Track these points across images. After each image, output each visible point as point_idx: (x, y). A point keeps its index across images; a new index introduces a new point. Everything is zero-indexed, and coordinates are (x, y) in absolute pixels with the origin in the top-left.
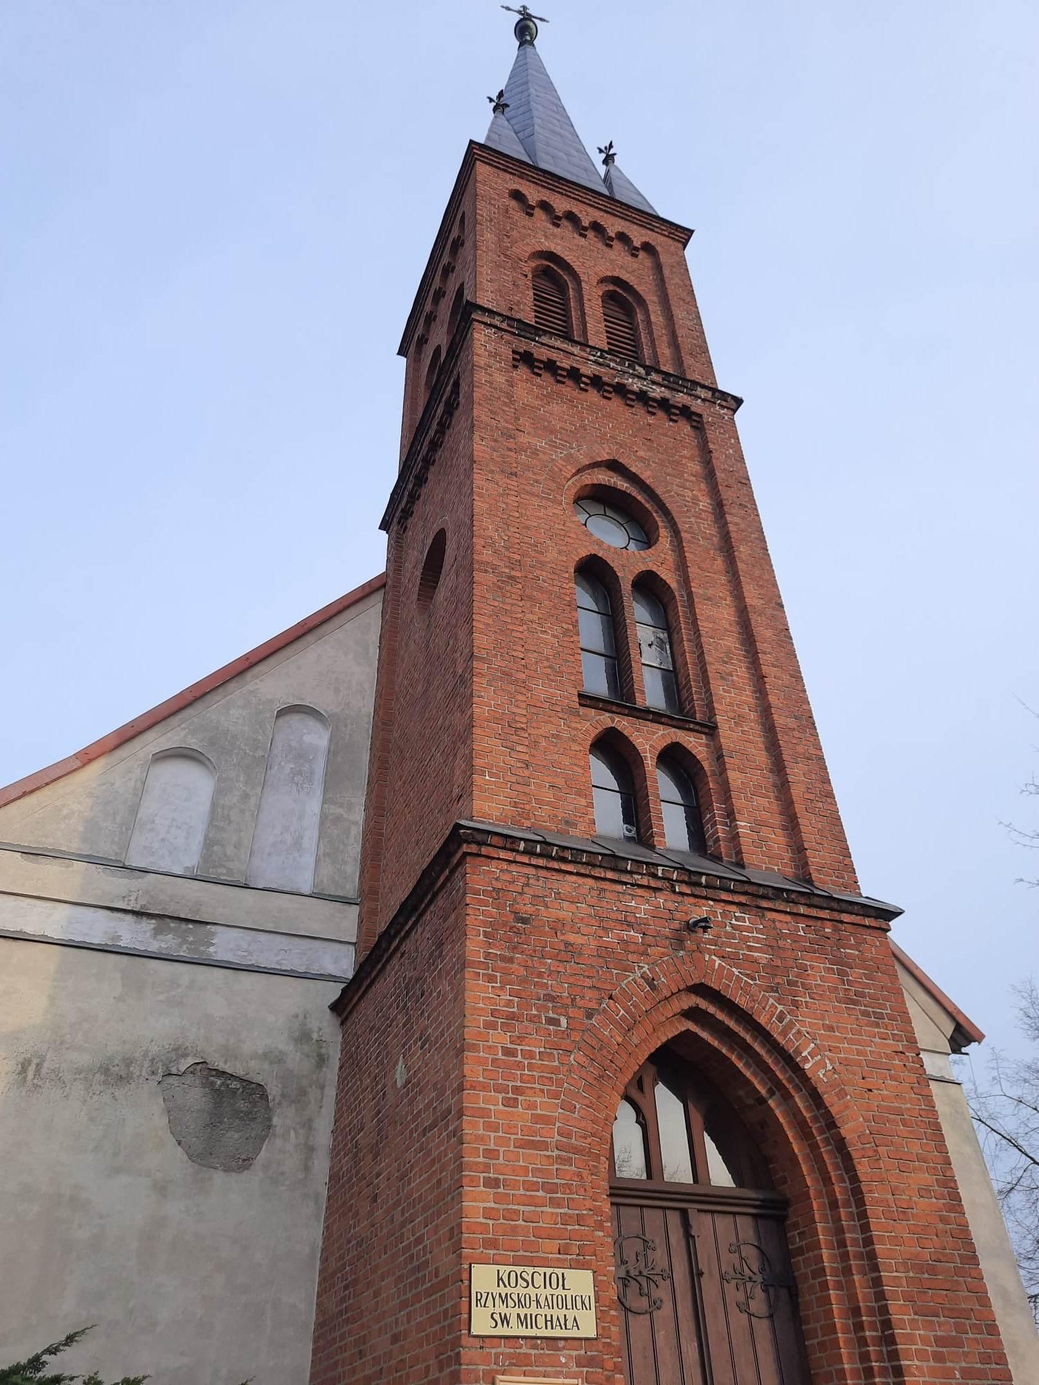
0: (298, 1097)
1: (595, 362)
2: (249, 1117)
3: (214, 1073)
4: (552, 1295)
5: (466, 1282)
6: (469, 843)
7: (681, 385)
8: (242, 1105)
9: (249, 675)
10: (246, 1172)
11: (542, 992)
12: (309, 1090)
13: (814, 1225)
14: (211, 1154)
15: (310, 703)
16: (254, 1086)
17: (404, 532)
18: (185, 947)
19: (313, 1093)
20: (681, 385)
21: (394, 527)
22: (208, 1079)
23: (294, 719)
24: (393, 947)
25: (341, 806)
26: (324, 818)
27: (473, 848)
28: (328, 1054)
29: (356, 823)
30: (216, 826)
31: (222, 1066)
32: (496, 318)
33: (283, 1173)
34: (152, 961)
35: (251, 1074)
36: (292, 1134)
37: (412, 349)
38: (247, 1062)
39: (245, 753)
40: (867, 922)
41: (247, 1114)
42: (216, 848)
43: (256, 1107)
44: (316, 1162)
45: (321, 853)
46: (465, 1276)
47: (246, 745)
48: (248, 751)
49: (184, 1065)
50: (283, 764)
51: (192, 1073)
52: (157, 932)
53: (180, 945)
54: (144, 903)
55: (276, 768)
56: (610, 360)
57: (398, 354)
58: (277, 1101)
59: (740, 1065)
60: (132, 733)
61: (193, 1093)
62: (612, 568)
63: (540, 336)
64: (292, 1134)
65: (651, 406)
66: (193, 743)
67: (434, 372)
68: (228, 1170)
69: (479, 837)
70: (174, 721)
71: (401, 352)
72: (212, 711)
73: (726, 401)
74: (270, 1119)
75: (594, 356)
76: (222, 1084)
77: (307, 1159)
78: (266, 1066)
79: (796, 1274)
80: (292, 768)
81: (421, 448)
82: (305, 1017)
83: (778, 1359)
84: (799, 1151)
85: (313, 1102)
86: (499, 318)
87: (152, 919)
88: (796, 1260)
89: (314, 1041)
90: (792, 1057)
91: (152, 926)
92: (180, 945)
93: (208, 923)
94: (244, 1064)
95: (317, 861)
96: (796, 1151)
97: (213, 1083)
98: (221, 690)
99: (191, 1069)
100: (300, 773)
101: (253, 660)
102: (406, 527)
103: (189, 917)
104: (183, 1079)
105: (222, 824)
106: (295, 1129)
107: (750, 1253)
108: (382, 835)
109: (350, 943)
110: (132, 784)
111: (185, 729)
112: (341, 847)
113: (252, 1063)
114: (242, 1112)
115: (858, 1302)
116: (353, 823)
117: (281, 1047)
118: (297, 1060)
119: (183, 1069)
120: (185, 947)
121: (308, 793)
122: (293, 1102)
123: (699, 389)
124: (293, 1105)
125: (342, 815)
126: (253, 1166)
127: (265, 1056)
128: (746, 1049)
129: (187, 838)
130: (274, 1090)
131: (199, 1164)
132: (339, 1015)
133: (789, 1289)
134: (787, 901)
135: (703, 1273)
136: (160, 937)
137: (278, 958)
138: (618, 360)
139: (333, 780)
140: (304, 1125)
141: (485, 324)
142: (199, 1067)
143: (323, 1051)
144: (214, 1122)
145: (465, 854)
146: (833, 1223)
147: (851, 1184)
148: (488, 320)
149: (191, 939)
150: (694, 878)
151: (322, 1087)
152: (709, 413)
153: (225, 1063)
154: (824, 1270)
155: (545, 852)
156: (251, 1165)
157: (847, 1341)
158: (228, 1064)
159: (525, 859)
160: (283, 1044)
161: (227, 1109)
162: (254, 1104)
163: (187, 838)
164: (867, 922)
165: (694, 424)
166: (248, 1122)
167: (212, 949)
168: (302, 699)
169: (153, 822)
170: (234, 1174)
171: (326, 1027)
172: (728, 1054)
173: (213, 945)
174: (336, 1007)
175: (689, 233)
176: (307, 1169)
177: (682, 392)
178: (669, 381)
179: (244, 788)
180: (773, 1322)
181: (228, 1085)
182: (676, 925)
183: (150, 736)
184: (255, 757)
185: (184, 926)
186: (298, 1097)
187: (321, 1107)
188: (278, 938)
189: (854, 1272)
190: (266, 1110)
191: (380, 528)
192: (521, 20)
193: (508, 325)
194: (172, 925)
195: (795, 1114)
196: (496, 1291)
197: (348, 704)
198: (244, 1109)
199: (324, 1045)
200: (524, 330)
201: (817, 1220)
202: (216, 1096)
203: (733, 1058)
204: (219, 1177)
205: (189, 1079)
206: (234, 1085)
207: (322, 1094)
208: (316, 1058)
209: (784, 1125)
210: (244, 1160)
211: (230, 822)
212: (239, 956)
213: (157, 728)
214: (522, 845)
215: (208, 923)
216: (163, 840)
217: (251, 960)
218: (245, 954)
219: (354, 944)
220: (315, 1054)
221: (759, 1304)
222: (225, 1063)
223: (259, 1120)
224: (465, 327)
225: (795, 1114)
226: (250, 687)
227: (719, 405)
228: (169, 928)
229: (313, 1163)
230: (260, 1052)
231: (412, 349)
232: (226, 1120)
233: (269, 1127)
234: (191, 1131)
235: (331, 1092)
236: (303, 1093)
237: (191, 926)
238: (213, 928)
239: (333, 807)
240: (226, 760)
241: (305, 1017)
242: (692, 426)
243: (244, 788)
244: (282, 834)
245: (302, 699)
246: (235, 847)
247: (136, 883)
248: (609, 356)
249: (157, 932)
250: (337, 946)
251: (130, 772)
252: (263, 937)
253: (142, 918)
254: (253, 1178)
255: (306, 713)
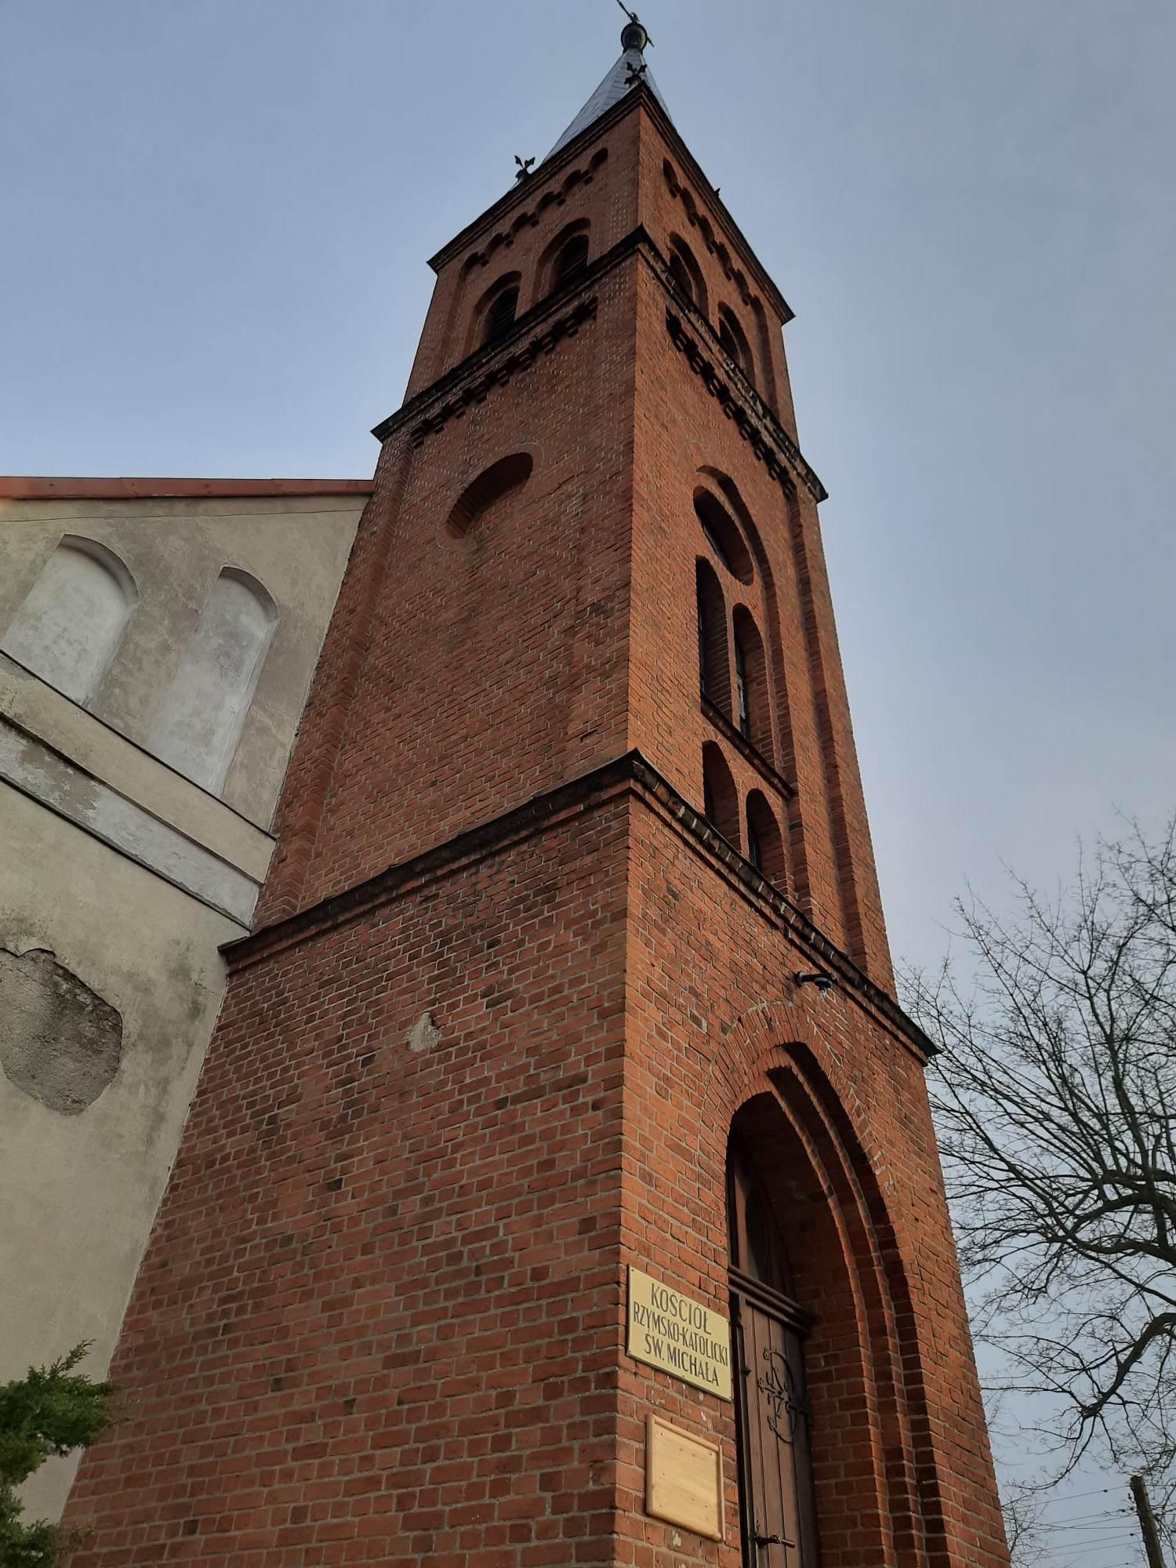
0: (160, 1046)
1: (727, 372)
2: (93, 1047)
3: (61, 972)
4: (696, 1334)
5: (623, 1287)
6: (637, 780)
7: (786, 447)
8: (88, 1029)
9: (204, 505)
10: (74, 1116)
11: (688, 983)
12: (174, 1041)
13: (856, 1348)
14: (33, 1077)
15: (262, 579)
16: (107, 1009)
17: (416, 447)
18: (57, 794)
19: (177, 1048)
20: (786, 447)
21: (403, 435)
22: (51, 976)
23: (235, 590)
24: (403, 890)
25: (271, 717)
26: (248, 723)
27: (639, 788)
28: (205, 1006)
29: (283, 746)
30: (122, 664)
31: (73, 967)
32: (660, 263)
33: (120, 1136)
34: (13, 791)
35: (107, 992)
36: (142, 1090)
37: (457, 264)
38: (106, 975)
39: (177, 595)
40: (914, 1048)
41: (91, 1042)
42: (117, 691)
43: (104, 1038)
44: (162, 1135)
45: (238, 759)
46: (623, 1279)
47: (179, 586)
48: (180, 595)
49: (26, 945)
50: (211, 633)
51: (33, 959)
52: (26, 758)
53: (52, 789)
54: (21, 712)
55: (202, 634)
56: (739, 379)
57: (428, 262)
58: (132, 1040)
59: (809, 1151)
60: (49, 492)
61: (29, 986)
62: (719, 583)
63: (690, 311)
64: (142, 1090)
65: (760, 449)
66: (118, 548)
67: (490, 299)
68: (51, 1106)
69: (649, 779)
70: (104, 508)
71: (435, 263)
72: (153, 522)
73: (815, 488)
74: (118, 1060)
75: (728, 365)
76: (68, 991)
77: (153, 1129)
78: (129, 990)
79: (813, 1402)
80: (220, 645)
81: (487, 362)
82: (188, 949)
83: (796, 1492)
84: (850, 1264)
85: (175, 1057)
86: (662, 266)
87: (22, 738)
88: (814, 1386)
89: (192, 982)
90: (866, 1158)
91: (21, 748)
92: (52, 789)
93: (92, 777)
94: (102, 976)
95: (231, 770)
96: (847, 1262)
97: (56, 985)
98: (166, 504)
99: (33, 955)
100: (227, 654)
101: (215, 491)
102: (421, 443)
103: (73, 758)
104: (19, 963)
105: (131, 666)
106: (146, 1085)
107: (778, 1363)
108: (332, 768)
109: (255, 882)
110: (30, 556)
111: (112, 526)
112: (262, 765)
113: (112, 979)
114: (85, 1037)
115: (901, 1443)
116: (281, 743)
117: (152, 974)
118: (167, 999)
119: (23, 949)
120: (57, 794)
121: (231, 685)
122: (151, 1048)
123: (798, 460)
124: (151, 1052)
125: (270, 729)
126: (84, 1112)
127: (130, 976)
128: (818, 1135)
129: (77, 662)
130: (131, 1024)
131: (17, 1085)
132: (229, 963)
133: (806, 1416)
134: (865, 995)
135: (750, 1371)
136: (27, 766)
137: (170, 862)
138: (746, 385)
139: (267, 682)
140: (159, 1084)
141: (648, 262)
142: (44, 956)
143: (200, 999)
144: (47, 1037)
145: (631, 791)
146: (872, 1351)
147: (896, 1313)
148: (652, 262)
149: (67, 787)
150: (807, 931)
151: (190, 1045)
152: (802, 491)
153: (79, 963)
154: (865, 1402)
155: (698, 831)
156: (81, 1111)
157: (881, 1483)
158: (81, 968)
159: (679, 828)
160: (153, 969)
161: (67, 1025)
162: (102, 1032)
163: (77, 662)
164: (914, 1048)
165: (787, 492)
166: (89, 1053)
167: (90, 813)
168: (254, 570)
169: (39, 619)
170: (57, 1114)
171: (212, 972)
172: (800, 1134)
173: (94, 808)
174: (228, 952)
175: (792, 316)
176: (150, 1141)
177: (785, 454)
178: (778, 436)
179: (166, 637)
180: (793, 1446)
181: (75, 995)
182: (786, 972)
183: (69, 509)
184: (187, 607)
185: (61, 766)
186: (160, 1046)
187: (183, 1068)
188: (174, 837)
189: (898, 1409)
190: (116, 1047)
191: (372, 431)
192: (629, 26)
193: (667, 278)
194: (47, 758)
195: (852, 1222)
196: (648, 1305)
197: (303, 604)
198: (89, 1035)
199: (203, 992)
200: (678, 295)
201: (861, 1344)
202: (57, 1003)
203: (804, 1140)
204: (37, 1111)
205: (28, 967)
206: (84, 998)
207: (188, 1052)
208: (190, 1005)
209: (839, 1230)
210: (74, 1101)
211: (140, 669)
212: (122, 837)
213: (78, 505)
214: (682, 812)
215: (92, 777)
216: (47, 648)
217: (135, 849)
218: (131, 838)
219: (261, 885)
220: (190, 999)
221: (783, 1426)
222: (79, 963)
223: (104, 1056)
224: (622, 254)
225: (852, 1222)
226: (200, 520)
227: (809, 487)
228: (43, 760)
229: (159, 1136)
230: (125, 969)
231: (457, 264)
232: (63, 1039)
233: (115, 1070)
234: (14, 1036)
235: (200, 1054)
236: (166, 1042)
237: (70, 771)
238: (98, 787)
239: (262, 713)
240: (153, 592)
241: (188, 949)
242: (784, 493)
243: (166, 637)
244: (191, 716)
245: (254, 570)
246: (140, 701)
247: (15, 682)
248: (740, 375)
249: (26, 758)
250: (240, 879)
251: (31, 540)
252: (156, 827)
253: (10, 730)
254: (84, 1126)
255: (247, 587)
